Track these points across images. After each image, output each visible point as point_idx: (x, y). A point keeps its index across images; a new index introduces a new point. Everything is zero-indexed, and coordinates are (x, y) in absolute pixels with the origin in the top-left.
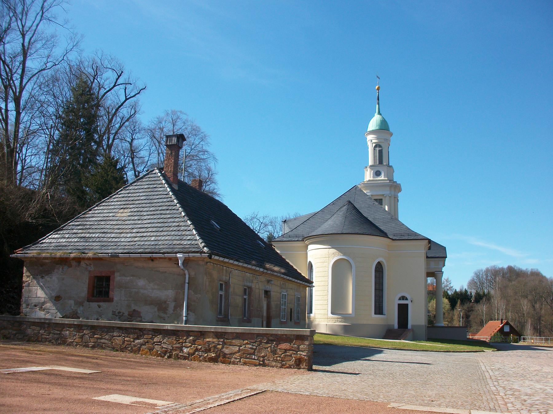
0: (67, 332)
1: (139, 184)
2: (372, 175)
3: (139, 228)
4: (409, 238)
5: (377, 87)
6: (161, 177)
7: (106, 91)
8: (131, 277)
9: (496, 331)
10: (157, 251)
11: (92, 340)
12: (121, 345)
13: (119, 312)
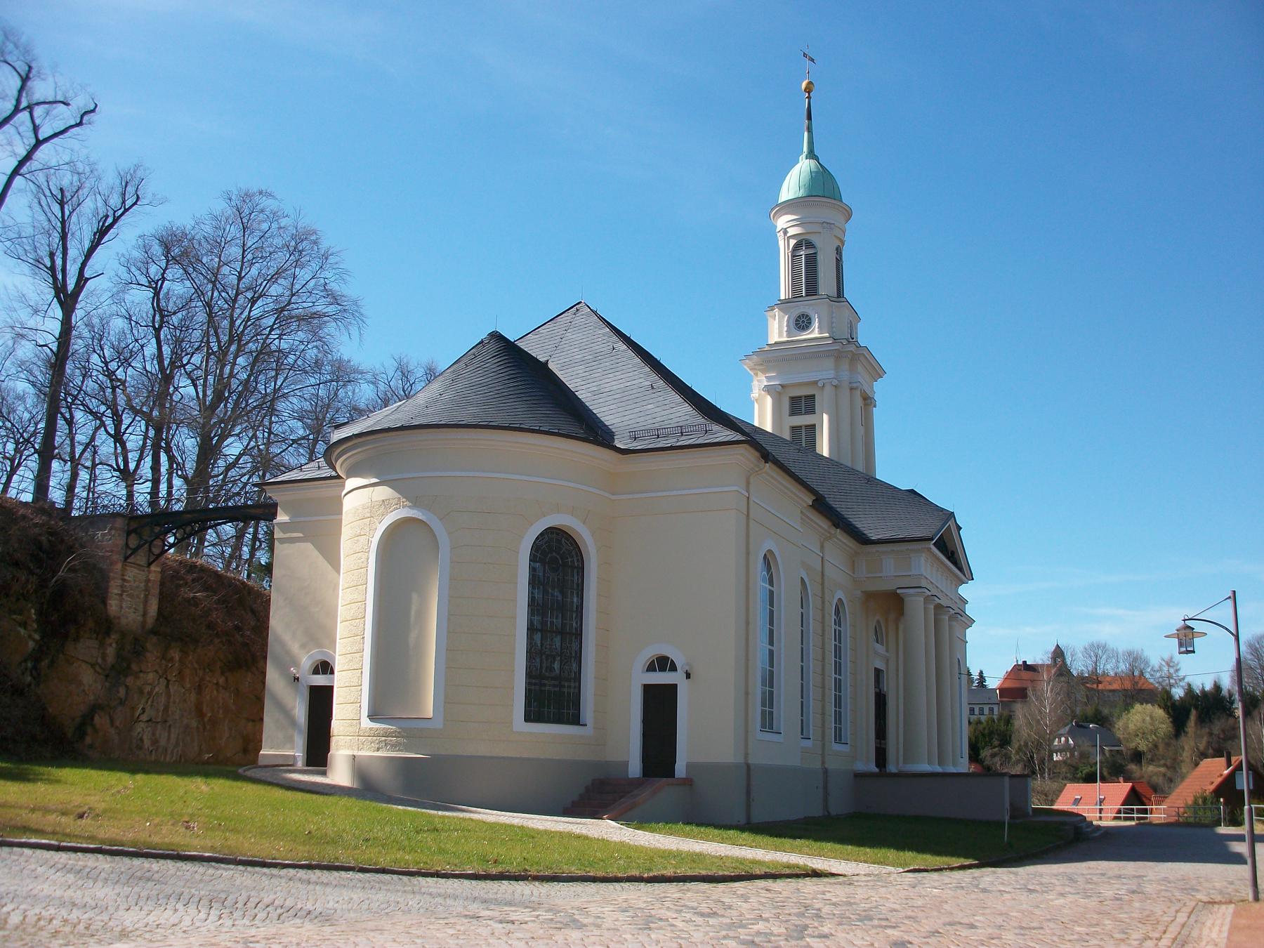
2: (785, 329)
5: (804, 85)
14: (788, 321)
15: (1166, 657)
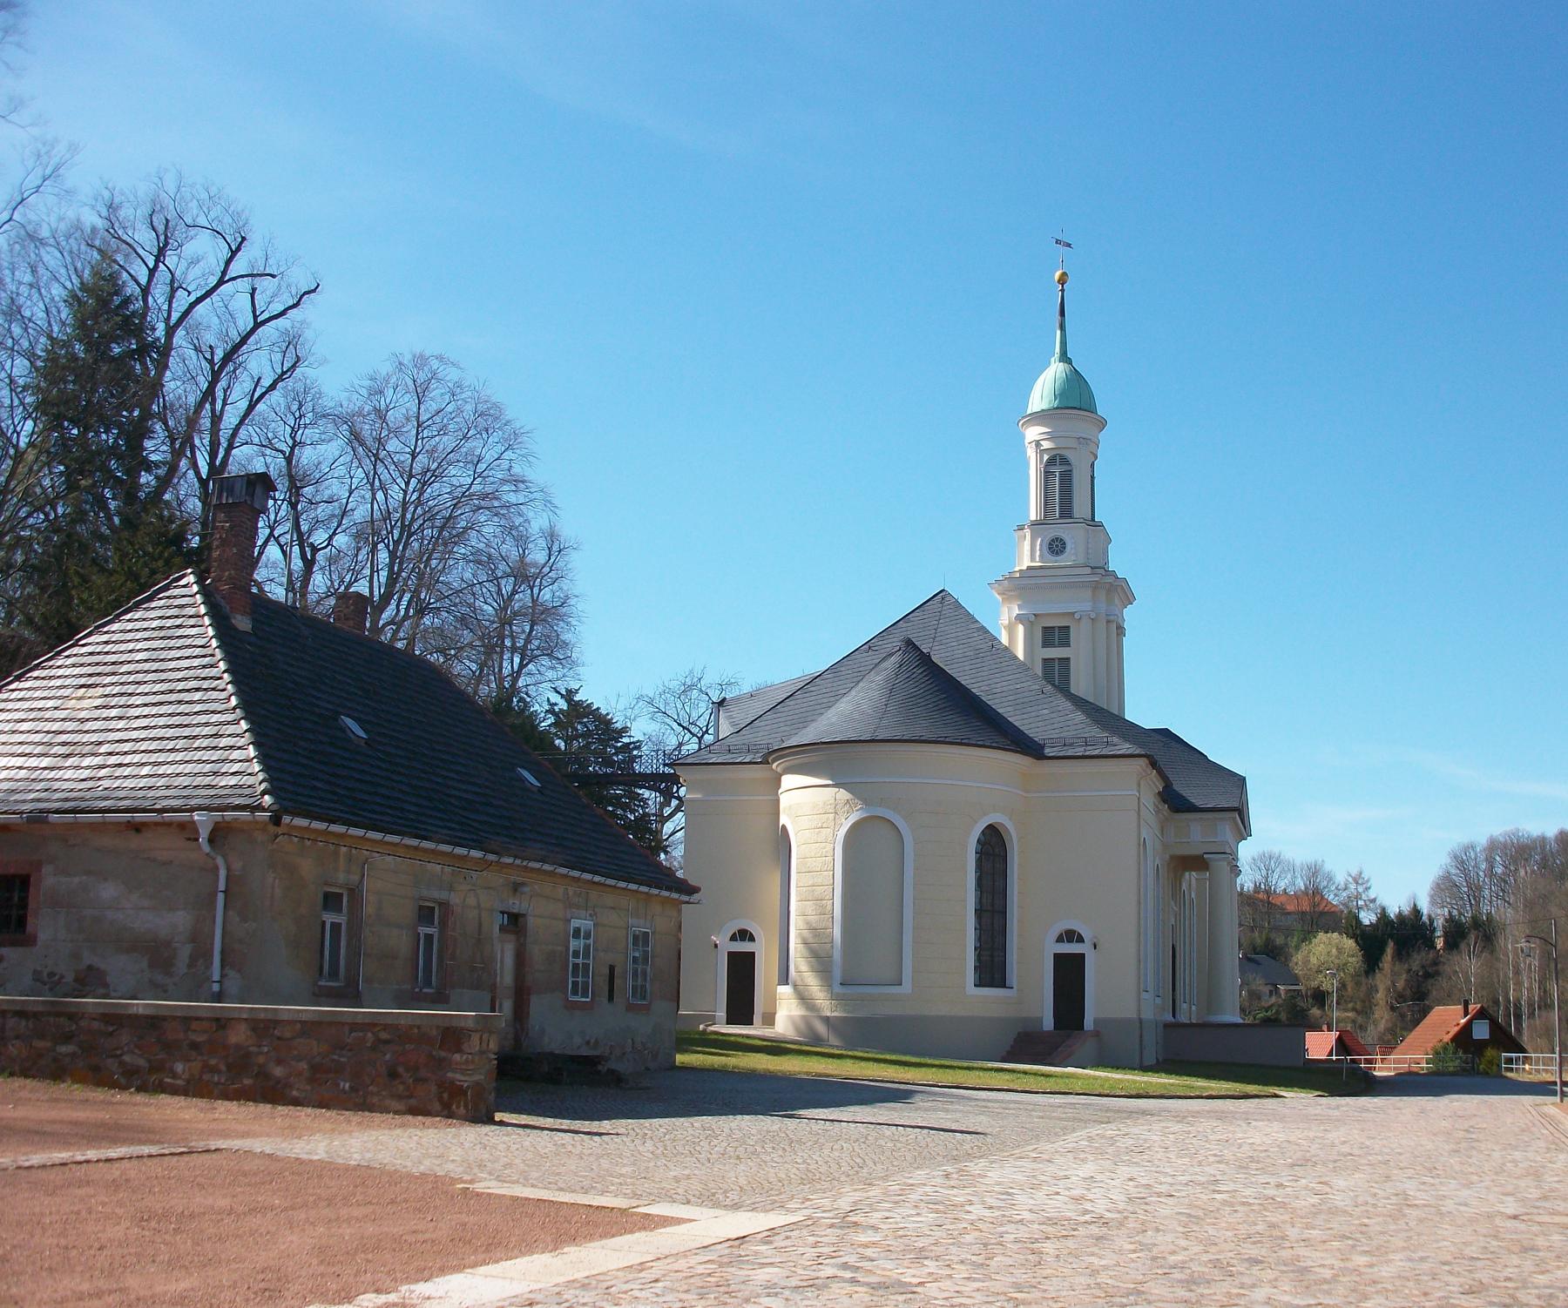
1: (138, 615)
2: (1038, 553)
3: (117, 741)
4: (1087, 753)
5: (1057, 275)
6: (198, 596)
7: (192, 298)
9: (1447, 1038)
10: (146, 804)
13: (51, 974)
15: (1354, 872)
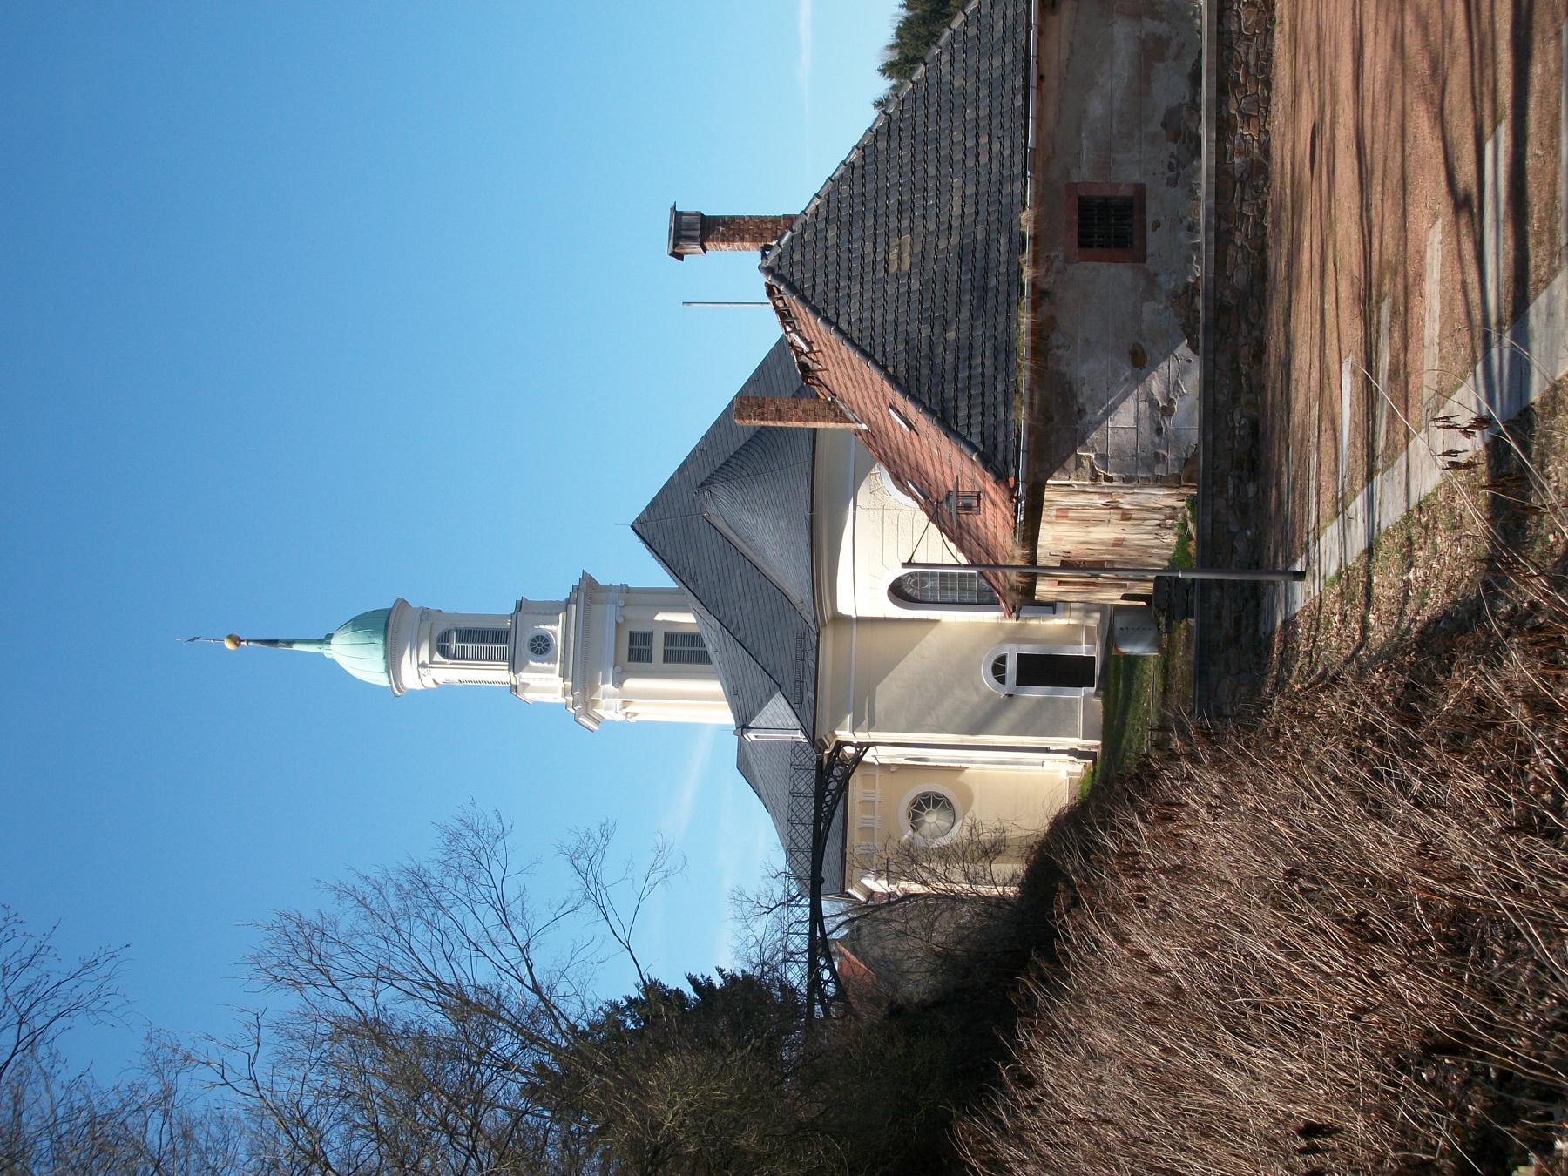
0: (1237, 160)
2: (546, 665)
5: (229, 645)
8: (1083, 135)
11: (1251, 89)
12: (1259, 11)
14: (536, 661)
